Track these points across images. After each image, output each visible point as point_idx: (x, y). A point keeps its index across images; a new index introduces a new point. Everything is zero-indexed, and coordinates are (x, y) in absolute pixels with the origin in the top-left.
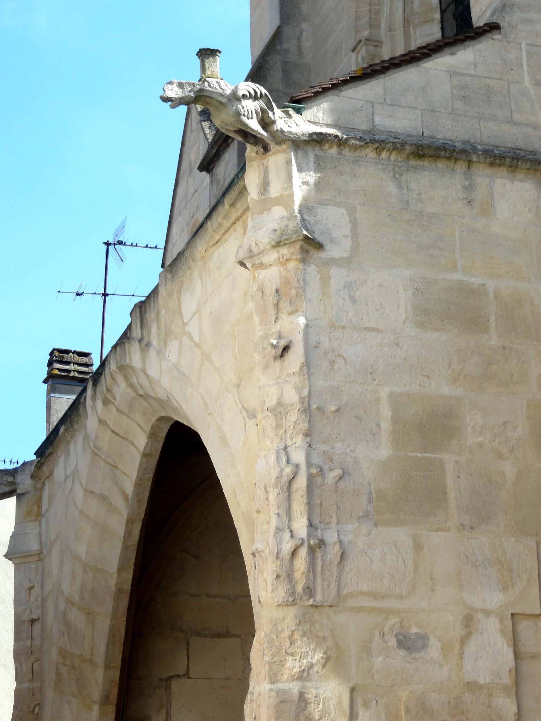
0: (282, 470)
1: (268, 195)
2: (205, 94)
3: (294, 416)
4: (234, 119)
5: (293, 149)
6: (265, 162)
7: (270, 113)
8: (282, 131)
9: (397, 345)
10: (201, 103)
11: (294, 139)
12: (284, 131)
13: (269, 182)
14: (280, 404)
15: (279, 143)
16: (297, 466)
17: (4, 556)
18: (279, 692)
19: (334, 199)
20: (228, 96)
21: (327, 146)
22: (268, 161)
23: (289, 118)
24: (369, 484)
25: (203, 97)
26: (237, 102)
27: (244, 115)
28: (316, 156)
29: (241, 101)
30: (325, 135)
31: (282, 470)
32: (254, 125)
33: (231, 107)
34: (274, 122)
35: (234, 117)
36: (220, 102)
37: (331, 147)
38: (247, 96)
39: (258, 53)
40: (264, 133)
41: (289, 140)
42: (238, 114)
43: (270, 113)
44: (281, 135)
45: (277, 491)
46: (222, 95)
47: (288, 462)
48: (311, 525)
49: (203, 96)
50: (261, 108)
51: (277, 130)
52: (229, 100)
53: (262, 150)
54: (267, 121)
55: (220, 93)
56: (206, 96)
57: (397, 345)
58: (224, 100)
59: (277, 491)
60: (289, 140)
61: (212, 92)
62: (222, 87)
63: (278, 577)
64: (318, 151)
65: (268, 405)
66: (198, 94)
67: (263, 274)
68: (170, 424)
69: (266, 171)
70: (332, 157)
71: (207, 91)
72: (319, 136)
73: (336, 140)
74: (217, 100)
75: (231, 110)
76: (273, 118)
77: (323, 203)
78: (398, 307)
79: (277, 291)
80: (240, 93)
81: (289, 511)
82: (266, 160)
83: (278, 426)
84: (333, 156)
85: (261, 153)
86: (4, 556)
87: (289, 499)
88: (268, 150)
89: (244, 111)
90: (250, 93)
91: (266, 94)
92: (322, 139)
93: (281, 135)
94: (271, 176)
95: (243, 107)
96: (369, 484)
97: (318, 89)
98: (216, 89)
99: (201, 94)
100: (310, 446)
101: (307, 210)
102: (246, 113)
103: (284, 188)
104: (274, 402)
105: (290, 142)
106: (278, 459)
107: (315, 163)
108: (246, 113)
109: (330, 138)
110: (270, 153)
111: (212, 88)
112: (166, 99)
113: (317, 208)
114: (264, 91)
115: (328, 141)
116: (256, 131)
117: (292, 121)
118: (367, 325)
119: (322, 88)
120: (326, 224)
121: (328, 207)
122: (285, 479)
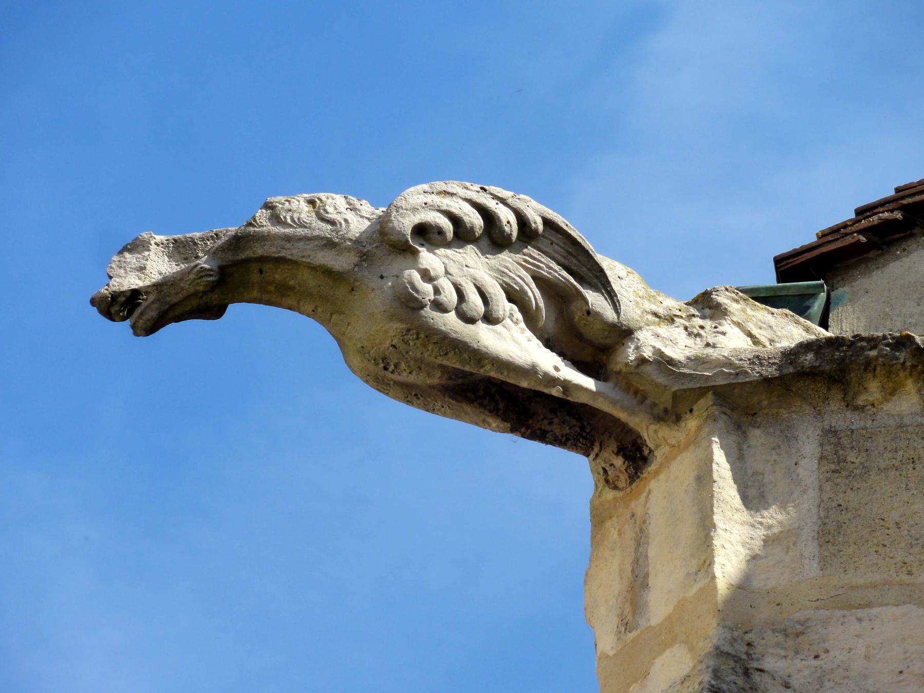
1: (643, 623)
2: (260, 250)
4: (398, 326)
5: (721, 424)
6: (637, 506)
7: (595, 299)
8: (664, 362)
10: (255, 294)
11: (720, 382)
12: (671, 361)
13: (646, 576)
15: (671, 414)
19: (904, 577)
20: (357, 241)
21: (873, 389)
22: (647, 497)
23: (712, 318)
25: (255, 267)
26: (399, 261)
27: (439, 306)
29: (415, 253)
30: (852, 344)
33: (374, 282)
34: (625, 333)
35: (392, 317)
36: (328, 272)
37: (891, 392)
38: (440, 231)
40: (589, 383)
41: (702, 392)
42: (409, 304)
43: (595, 299)
44: (662, 380)
46: (329, 244)
49: (248, 260)
50: (539, 280)
51: (642, 361)
52: (365, 257)
53: (619, 462)
54: (592, 332)
55: (318, 238)
56: (262, 259)
58: (341, 262)
60: (702, 392)
61: (288, 238)
62: (332, 215)
64: (838, 417)
66: (229, 257)
70: (901, 426)
71: (263, 238)
72: (827, 351)
73: (902, 355)
74: (314, 268)
75: (376, 296)
76: (609, 314)
77: (851, 603)
80: (406, 223)
82: (642, 498)
84: (907, 421)
85: (623, 477)
88: (645, 460)
89: (437, 291)
90: (456, 220)
91: (547, 222)
92: (843, 360)
93: (662, 380)
94: (653, 551)
95: (427, 276)
97: (886, 215)
98: (302, 225)
99: (243, 256)
101: (781, 638)
102: (450, 296)
103: (688, 574)
105: (707, 401)
107: (821, 458)
108: (450, 296)
109: (873, 353)
110: (652, 467)
111: (284, 224)
112: (117, 305)
113: (825, 622)
115: (869, 366)
116: (531, 371)
117: (726, 326)
119: (902, 208)
120: (865, 677)
121: (874, 611)
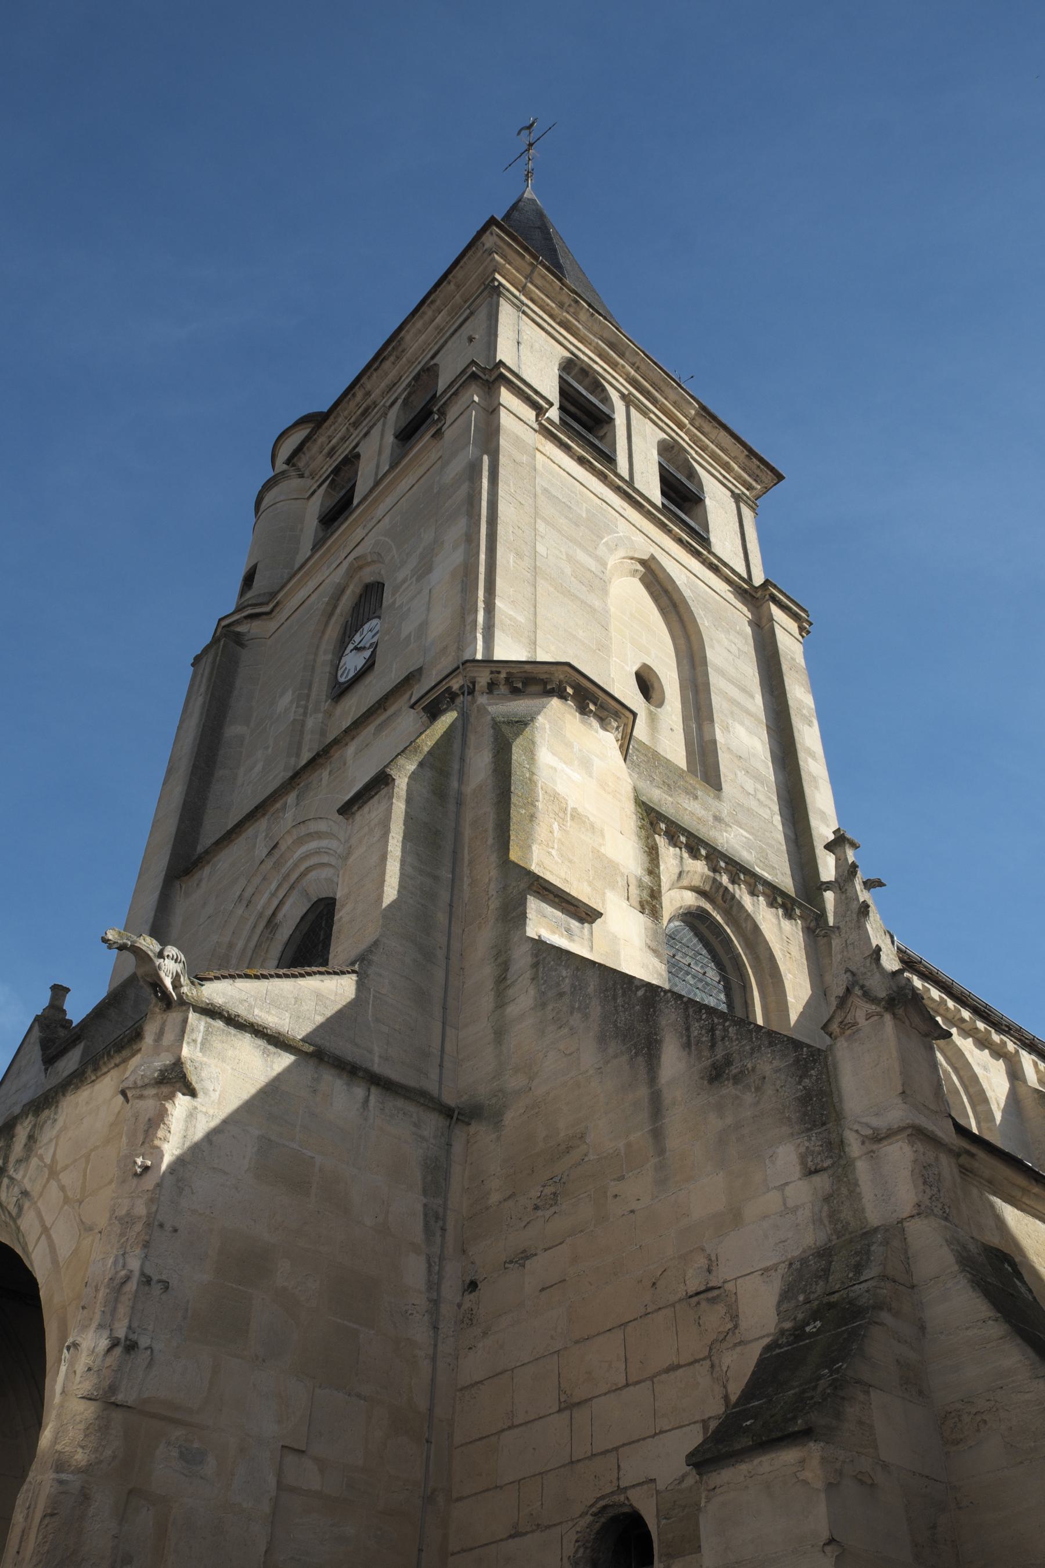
0: (117, 1273)
3: (138, 1227)
9: (237, 1189)
14: (128, 1214)
16: (131, 1271)
17: (67, 990)
18: (61, 1482)
24: (188, 1301)
28: (206, 1022)
31: (117, 1273)
32: (168, 982)
39: (115, 985)
45: (108, 1291)
47: (124, 1266)
48: (130, 1328)
57: (237, 1189)
59: (108, 1291)
63: (89, 1369)
65: (116, 1214)
67: (140, 1104)
68: (331, 895)
69: (164, 1024)
78: (244, 1157)
79: (149, 1120)
81: (114, 1310)
83: (122, 1235)
86: (67, 990)
87: (116, 1300)
94: (166, 1028)
96: (188, 1301)
100: (146, 1257)
104: (124, 1212)
106: (115, 1263)
114: (183, 959)
118: (215, 1166)
122: (117, 1281)
